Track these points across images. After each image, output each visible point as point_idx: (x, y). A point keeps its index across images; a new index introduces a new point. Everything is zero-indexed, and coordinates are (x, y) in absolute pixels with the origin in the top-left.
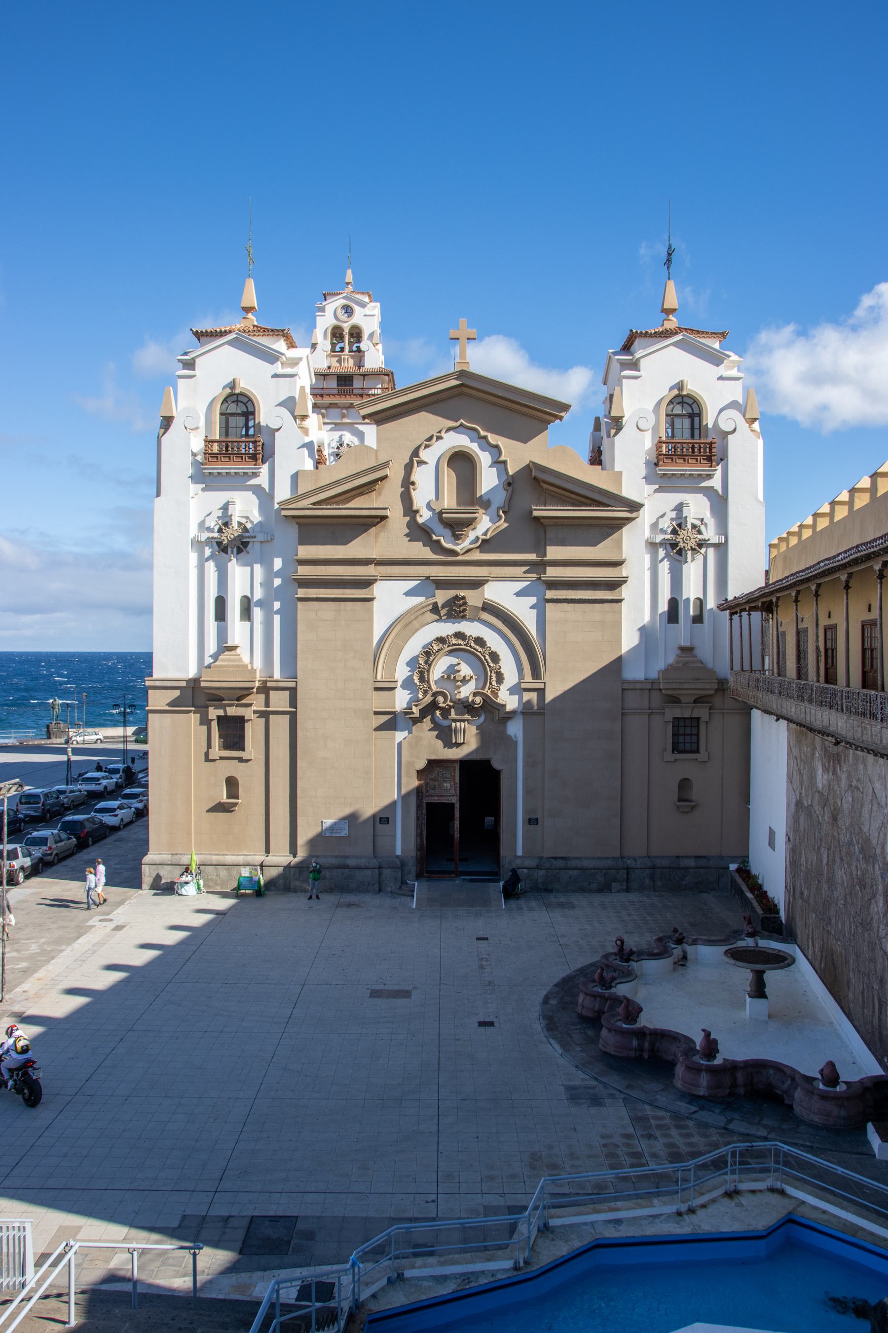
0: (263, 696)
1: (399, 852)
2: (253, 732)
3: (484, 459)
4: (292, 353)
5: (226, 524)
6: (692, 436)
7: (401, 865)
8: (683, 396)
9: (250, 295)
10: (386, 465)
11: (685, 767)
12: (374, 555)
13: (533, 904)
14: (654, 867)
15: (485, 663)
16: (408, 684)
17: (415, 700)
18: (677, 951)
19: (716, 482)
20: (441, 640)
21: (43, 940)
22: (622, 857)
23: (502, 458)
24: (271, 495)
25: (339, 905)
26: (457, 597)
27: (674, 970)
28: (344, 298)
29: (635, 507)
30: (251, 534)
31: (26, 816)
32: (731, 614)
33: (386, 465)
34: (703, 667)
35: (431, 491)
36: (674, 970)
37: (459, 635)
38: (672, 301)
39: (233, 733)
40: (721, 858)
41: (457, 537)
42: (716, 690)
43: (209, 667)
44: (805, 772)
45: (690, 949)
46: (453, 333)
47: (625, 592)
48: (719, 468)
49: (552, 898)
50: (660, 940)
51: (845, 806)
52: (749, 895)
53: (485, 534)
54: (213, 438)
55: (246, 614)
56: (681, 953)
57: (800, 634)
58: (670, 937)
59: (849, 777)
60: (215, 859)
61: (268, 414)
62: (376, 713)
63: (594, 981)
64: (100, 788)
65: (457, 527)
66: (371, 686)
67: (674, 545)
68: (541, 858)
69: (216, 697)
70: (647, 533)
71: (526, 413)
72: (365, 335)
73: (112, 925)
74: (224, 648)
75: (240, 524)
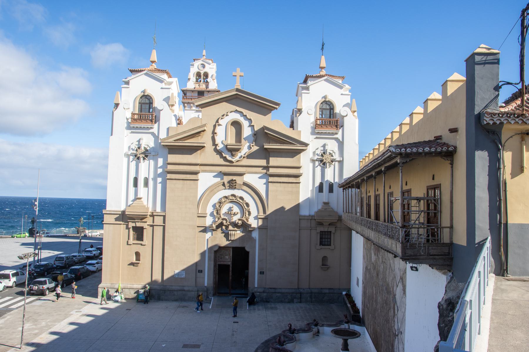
0: (152, 218)
1: (206, 285)
2: (147, 234)
3: (245, 124)
4: (171, 80)
5: (139, 148)
6: (330, 117)
7: (207, 290)
8: (326, 101)
9: (154, 56)
10: (205, 125)
11: (325, 251)
12: (199, 162)
13: (260, 307)
14: (311, 293)
15: (244, 207)
16: (212, 214)
17: (214, 222)
18: (315, 329)
19: (339, 136)
20: (226, 197)
21: (48, 320)
22: (298, 288)
23: (252, 124)
24: (158, 137)
25: (179, 307)
26: (232, 180)
27: (313, 337)
28: (202, 61)
29: (306, 145)
30: (149, 152)
31: (57, 266)
32: (343, 189)
33: (205, 125)
34: (333, 211)
35: (224, 136)
36: (313, 337)
37: (233, 195)
38: (323, 64)
39: (139, 233)
40: (339, 289)
41: (233, 155)
42: (338, 220)
43: (129, 206)
44: (368, 255)
45: (321, 329)
46: (234, 74)
47: (301, 179)
48: (341, 130)
49: (269, 305)
50: (308, 324)
51: (381, 270)
52: (349, 305)
53: (245, 154)
54: (135, 113)
55: (146, 184)
56: (317, 330)
57: (377, 197)
58: (312, 323)
59: (382, 258)
60: (129, 286)
61: (158, 103)
62: (198, 227)
63: (276, 342)
64: (92, 255)
65: (233, 151)
66: (196, 215)
67: (321, 161)
68: (265, 288)
69: (133, 218)
70: (311, 155)
71: (264, 107)
72: (210, 76)
73: (81, 314)
74: (137, 198)
75: (145, 147)
